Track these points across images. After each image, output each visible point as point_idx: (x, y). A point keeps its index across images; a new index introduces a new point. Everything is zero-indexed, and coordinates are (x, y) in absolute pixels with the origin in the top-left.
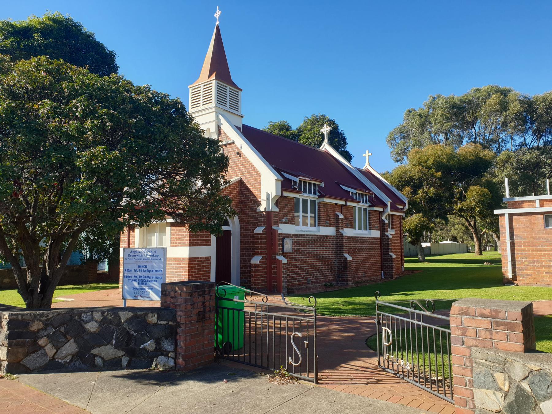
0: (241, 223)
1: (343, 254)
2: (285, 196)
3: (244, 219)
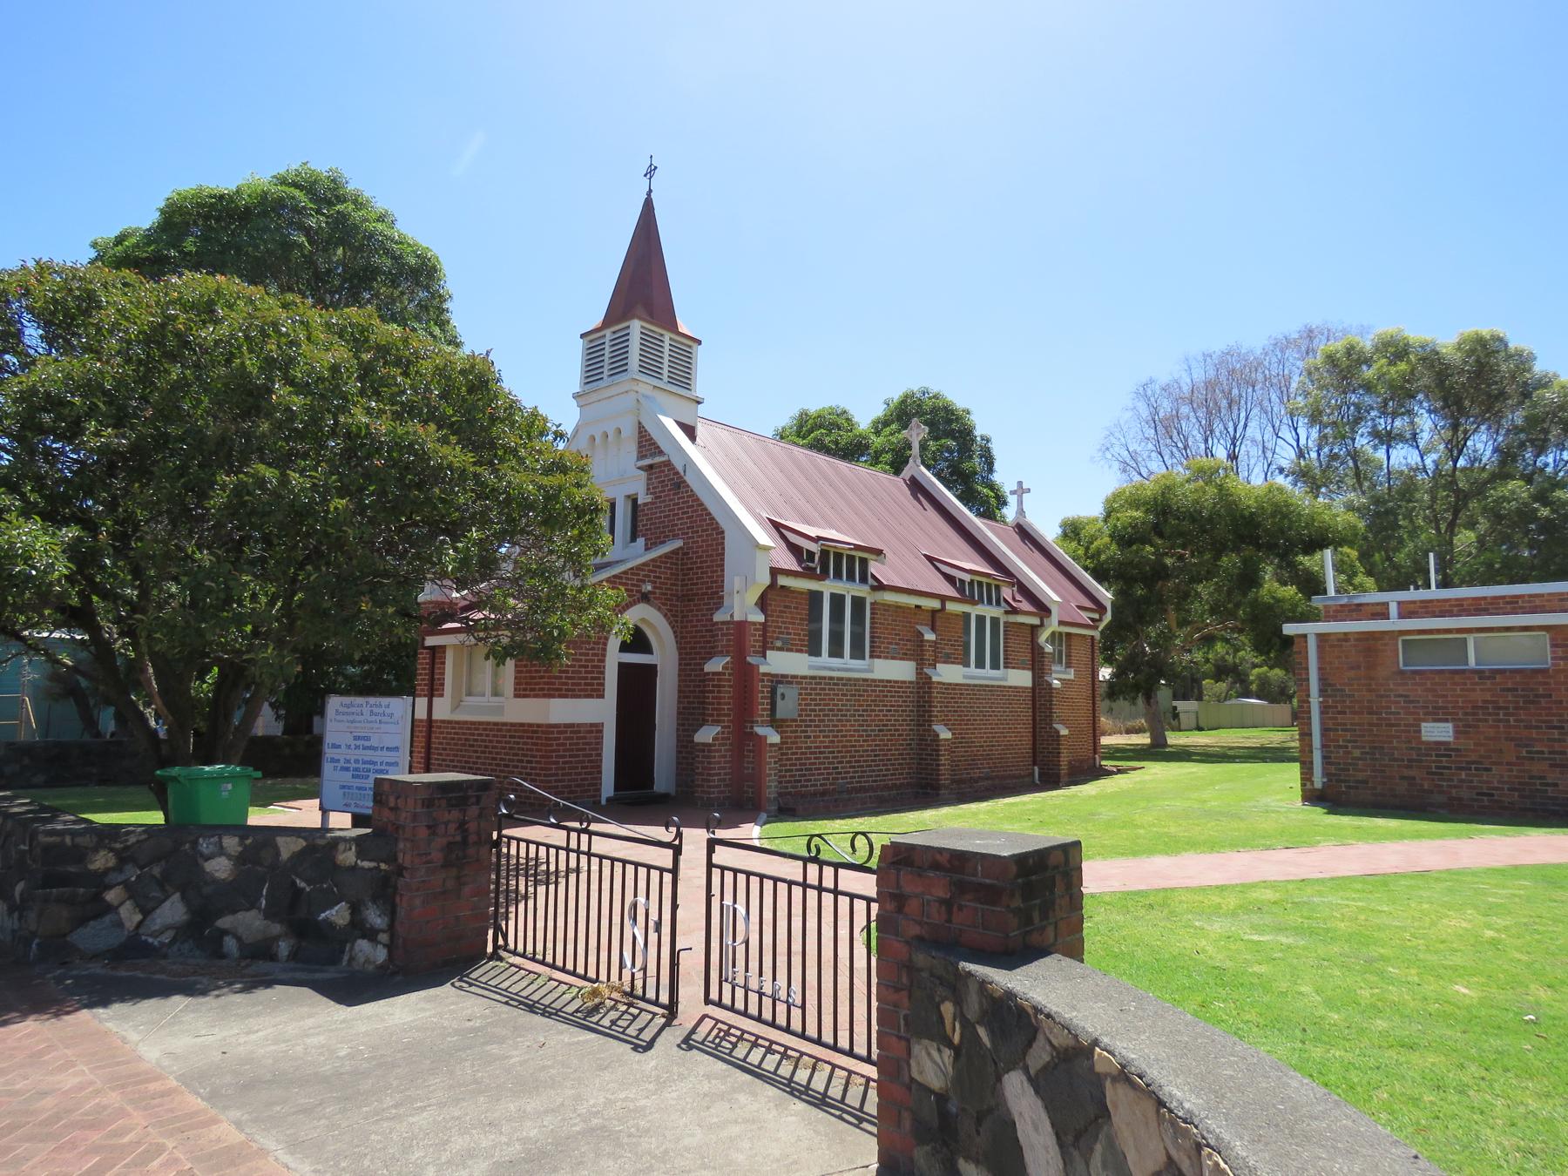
0: (680, 649)
1: (930, 726)
2: (782, 587)
3: (686, 638)
